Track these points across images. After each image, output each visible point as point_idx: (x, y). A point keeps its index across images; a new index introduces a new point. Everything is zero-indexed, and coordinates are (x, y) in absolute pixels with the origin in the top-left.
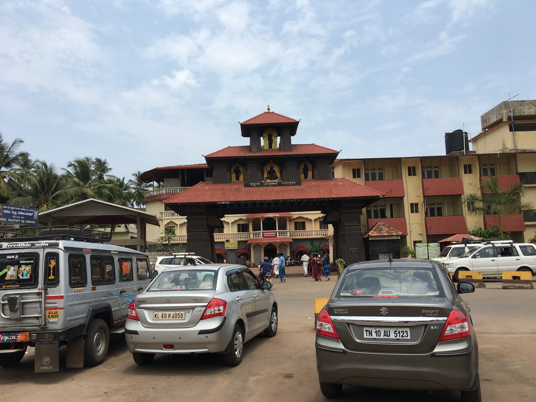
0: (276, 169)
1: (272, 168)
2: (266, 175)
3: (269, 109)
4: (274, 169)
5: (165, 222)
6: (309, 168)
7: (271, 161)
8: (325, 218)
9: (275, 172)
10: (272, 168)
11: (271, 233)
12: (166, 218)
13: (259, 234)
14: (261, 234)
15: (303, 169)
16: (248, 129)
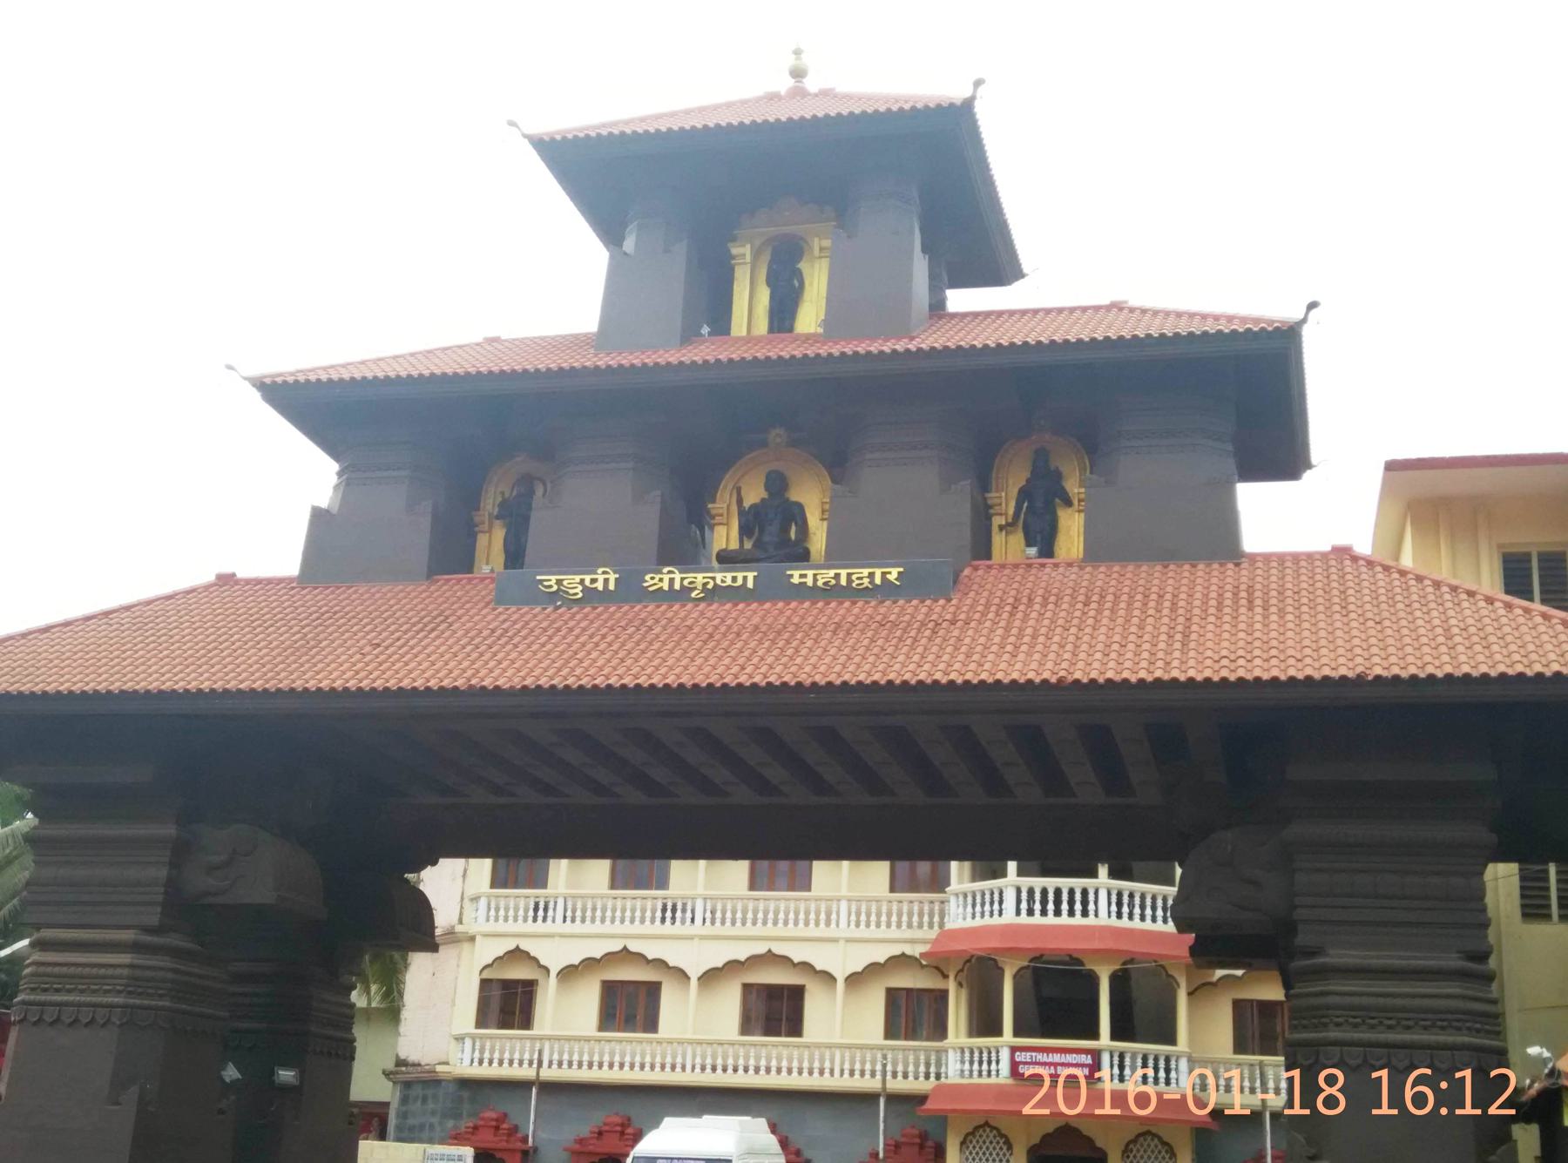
0: (811, 497)
1: (777, 485)
2: (725, 536)
3: (798, 74)
4: (795, 495)
5: (489, 951)
6: (1073, 487)
7: (777, 435)
8: (366, 1131)
9: (795, 514)
10: (777, 485)
11: (1059, 1057)
12: (491, 927)
13: (991, 1057)
14: (1005, 1055)
15: (1024, 494)
16: (610, 175)
